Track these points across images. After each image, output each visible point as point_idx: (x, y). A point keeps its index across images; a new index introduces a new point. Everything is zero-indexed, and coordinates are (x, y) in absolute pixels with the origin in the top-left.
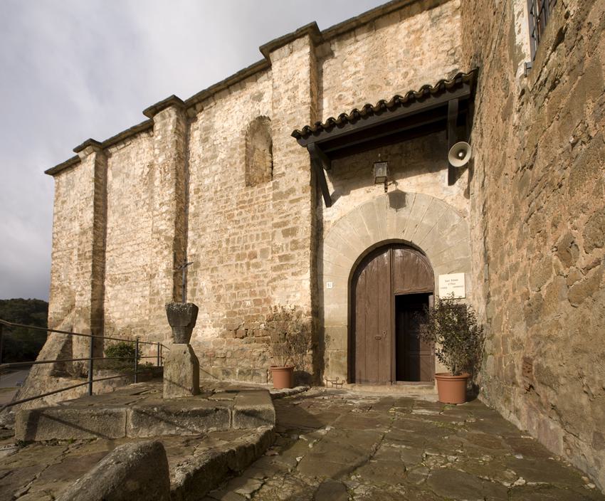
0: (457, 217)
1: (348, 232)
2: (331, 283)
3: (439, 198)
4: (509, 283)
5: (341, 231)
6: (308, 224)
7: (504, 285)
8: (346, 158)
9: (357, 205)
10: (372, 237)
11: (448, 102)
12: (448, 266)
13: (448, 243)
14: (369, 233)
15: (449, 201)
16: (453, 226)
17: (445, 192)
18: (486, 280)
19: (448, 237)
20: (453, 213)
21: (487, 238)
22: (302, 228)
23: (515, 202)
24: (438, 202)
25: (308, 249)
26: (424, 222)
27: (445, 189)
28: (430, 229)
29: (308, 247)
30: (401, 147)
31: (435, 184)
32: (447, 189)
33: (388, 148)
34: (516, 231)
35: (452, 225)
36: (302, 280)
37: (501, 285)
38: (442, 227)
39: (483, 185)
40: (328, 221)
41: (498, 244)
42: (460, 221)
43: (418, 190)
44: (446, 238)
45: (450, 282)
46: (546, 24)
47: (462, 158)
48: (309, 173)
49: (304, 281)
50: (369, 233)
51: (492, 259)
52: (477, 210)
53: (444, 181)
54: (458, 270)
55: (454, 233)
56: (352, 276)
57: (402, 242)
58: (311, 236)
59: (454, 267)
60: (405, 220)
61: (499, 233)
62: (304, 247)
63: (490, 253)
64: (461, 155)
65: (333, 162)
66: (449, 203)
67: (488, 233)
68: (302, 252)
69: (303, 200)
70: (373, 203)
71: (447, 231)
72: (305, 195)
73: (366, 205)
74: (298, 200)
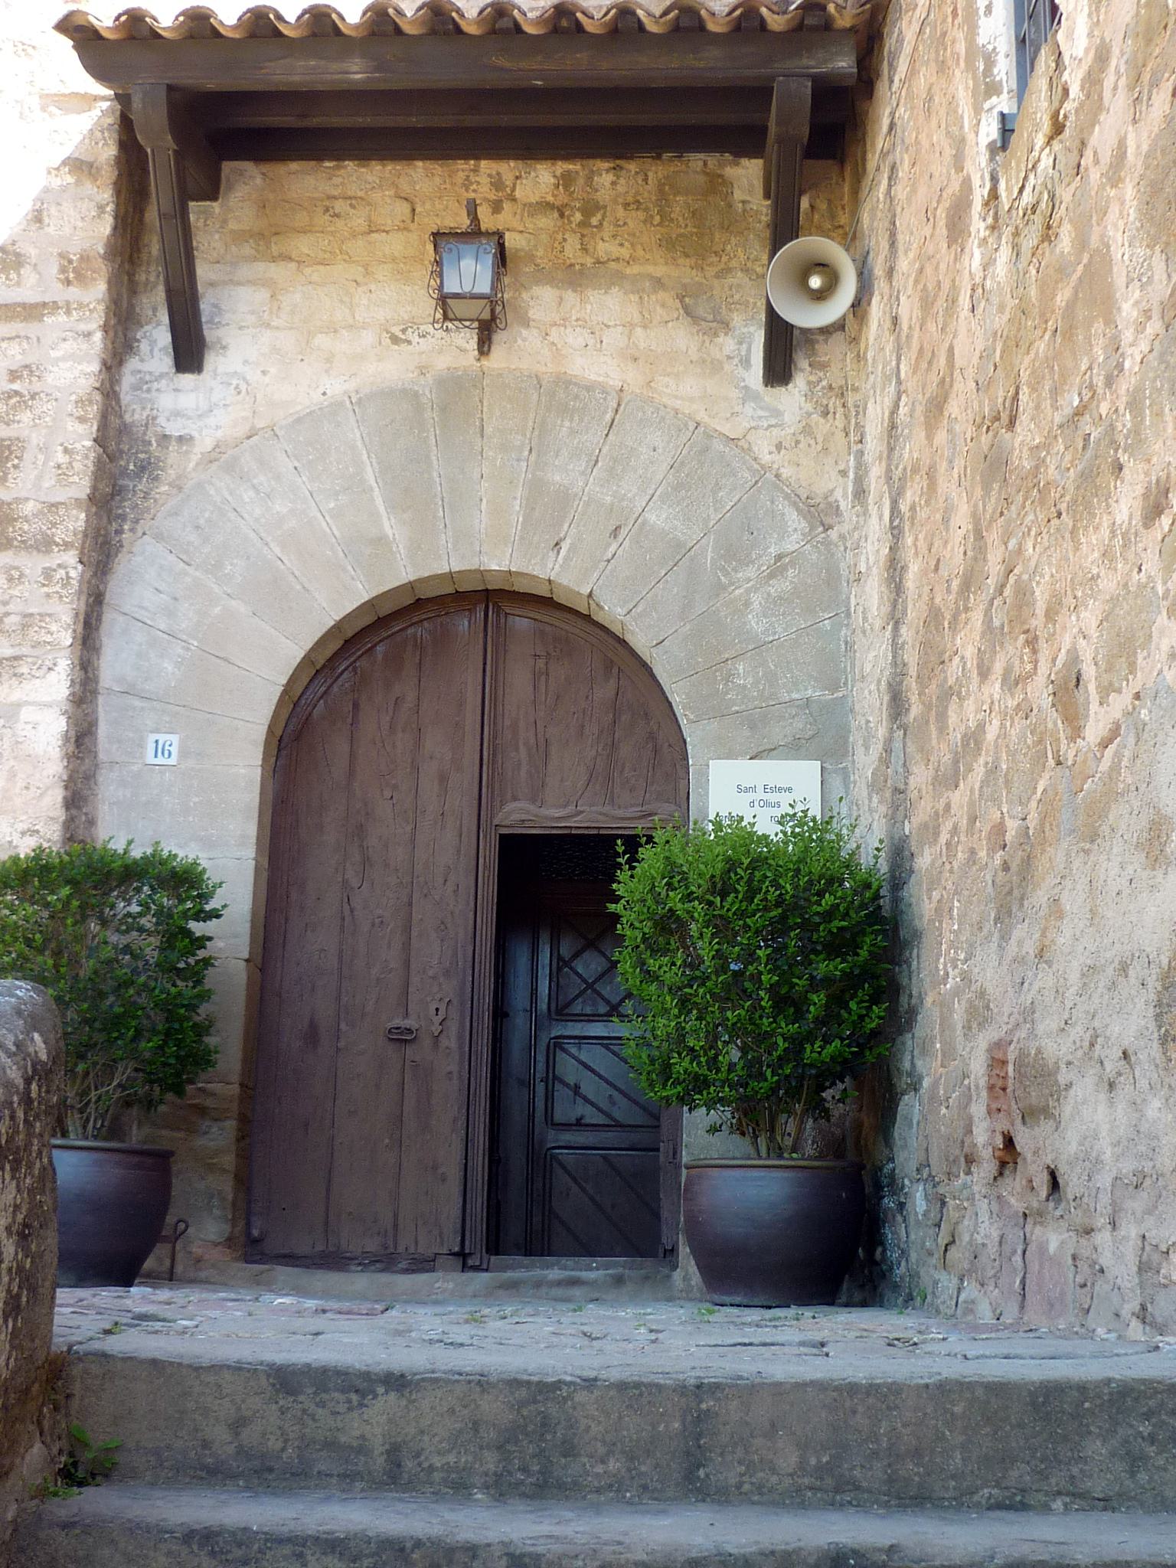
0: (794, 520)
1: (280, 507)
2: (175, 739)
3: (727, 429)
4: (958, 798)
5: (248, 495)
6: (82, 436)
7: (948, 807)
8: (294, 166)
9: (336, 386)
10: (401, 549)
11: (773, 78)
12: (752, 727)
13: (756, 624)
14: (390, 527)
15: (763, 449)
16: (779, 557)
17: (749, 409)
18: (352, 206)
19: (756, 600)
20: (782, 505)
21: (903, 630)
22: (44, 449)
23: (976, 519)
24: (718, 446)
25: (71, 558)
26: (651, 517)
27: (748, 395)
28: (679, 552)
29: (67, 546)
30: (567, 180)
31: (713, 367)
32: (756, 397)
33: (507, 169)
34: (977, 617)
35: (773, 550)
36: (19, 705)
37: (941, 806)
38: (734, 554)
39: (893, 426)
40: (180, 439)
41: (935, 657)
42: (809, 537)
43: (632, 378)
44: (747, 604)
45: (760, 795)
46: (1032, 70)
47: (821, 296)
48: (106, 195)
49: (26, 714)
50: (390, 527)
51: (915, 710)
52: (873, 510)
53: (746, 362)
54: (795, 749)
55: (780, 586)
56: (285, 713)
57: (543, 591)
58: (91, 498)
59: (779, 733)
60: (564, 499)
61: (934, 616)
62: (45, 544)
63: (911, 684)
64: (815, 282)
65: (227, 167)
66: (766, 458)
67: (905, 612)
68: (33, 564)
69: (61, 318)
70: (416, 395)
71: (751, 572)
72: (74, 293)
73: (388, 396)
74: (32, 312)
